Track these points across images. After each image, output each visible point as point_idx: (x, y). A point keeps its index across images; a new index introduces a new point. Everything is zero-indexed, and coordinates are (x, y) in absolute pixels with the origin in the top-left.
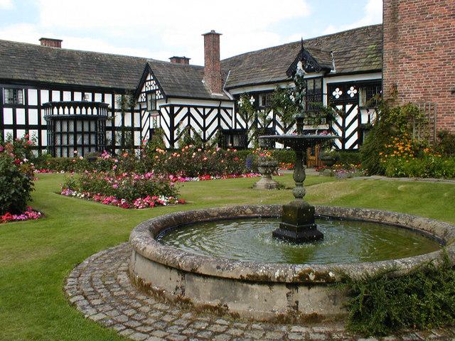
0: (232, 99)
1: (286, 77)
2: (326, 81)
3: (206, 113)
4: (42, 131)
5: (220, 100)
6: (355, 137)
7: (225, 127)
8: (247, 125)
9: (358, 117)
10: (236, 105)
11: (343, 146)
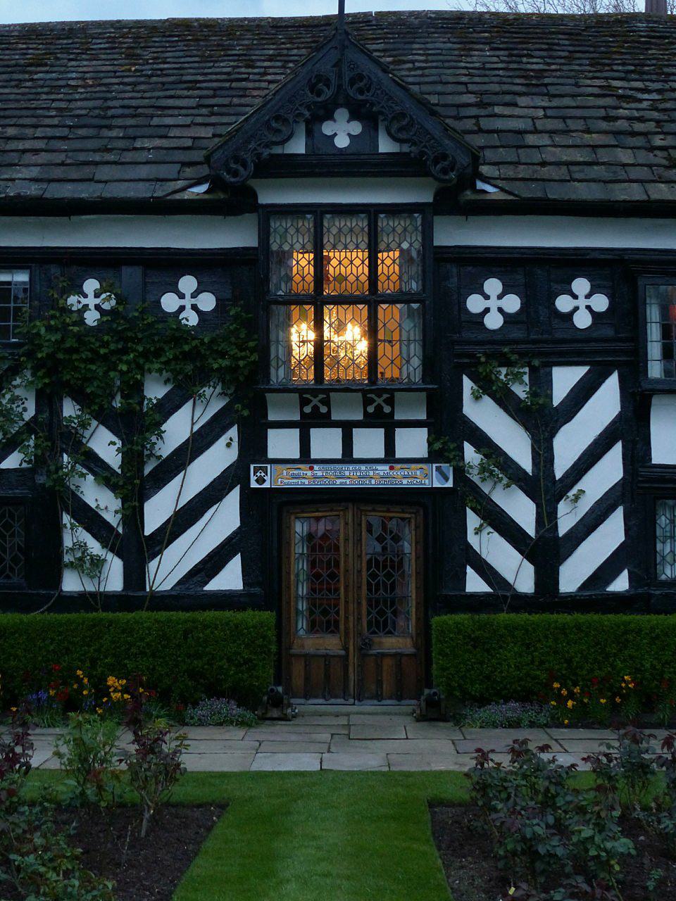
6: (611, 534)
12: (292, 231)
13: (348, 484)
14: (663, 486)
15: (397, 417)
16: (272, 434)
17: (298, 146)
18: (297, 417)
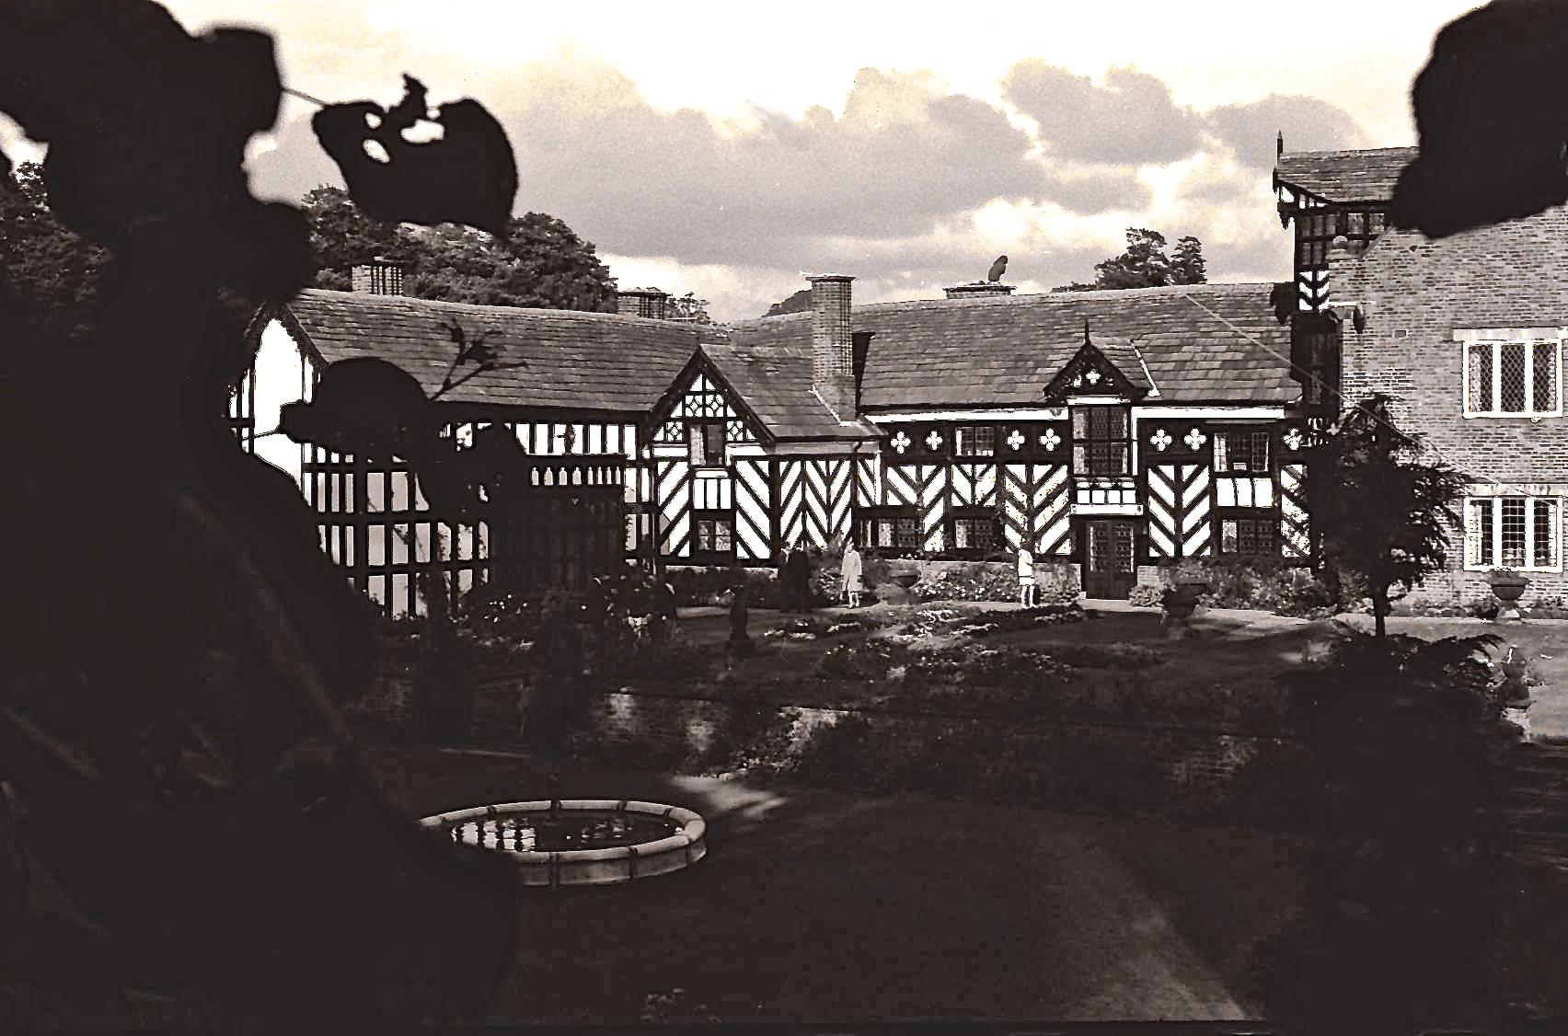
1: (1043, 399)
2: (1138, 413)
3: (925, 477)
4: (722, 415)
6: (1205, 532)
7: (864, 503)
9: (1211, 491)
16: (1080, 493)
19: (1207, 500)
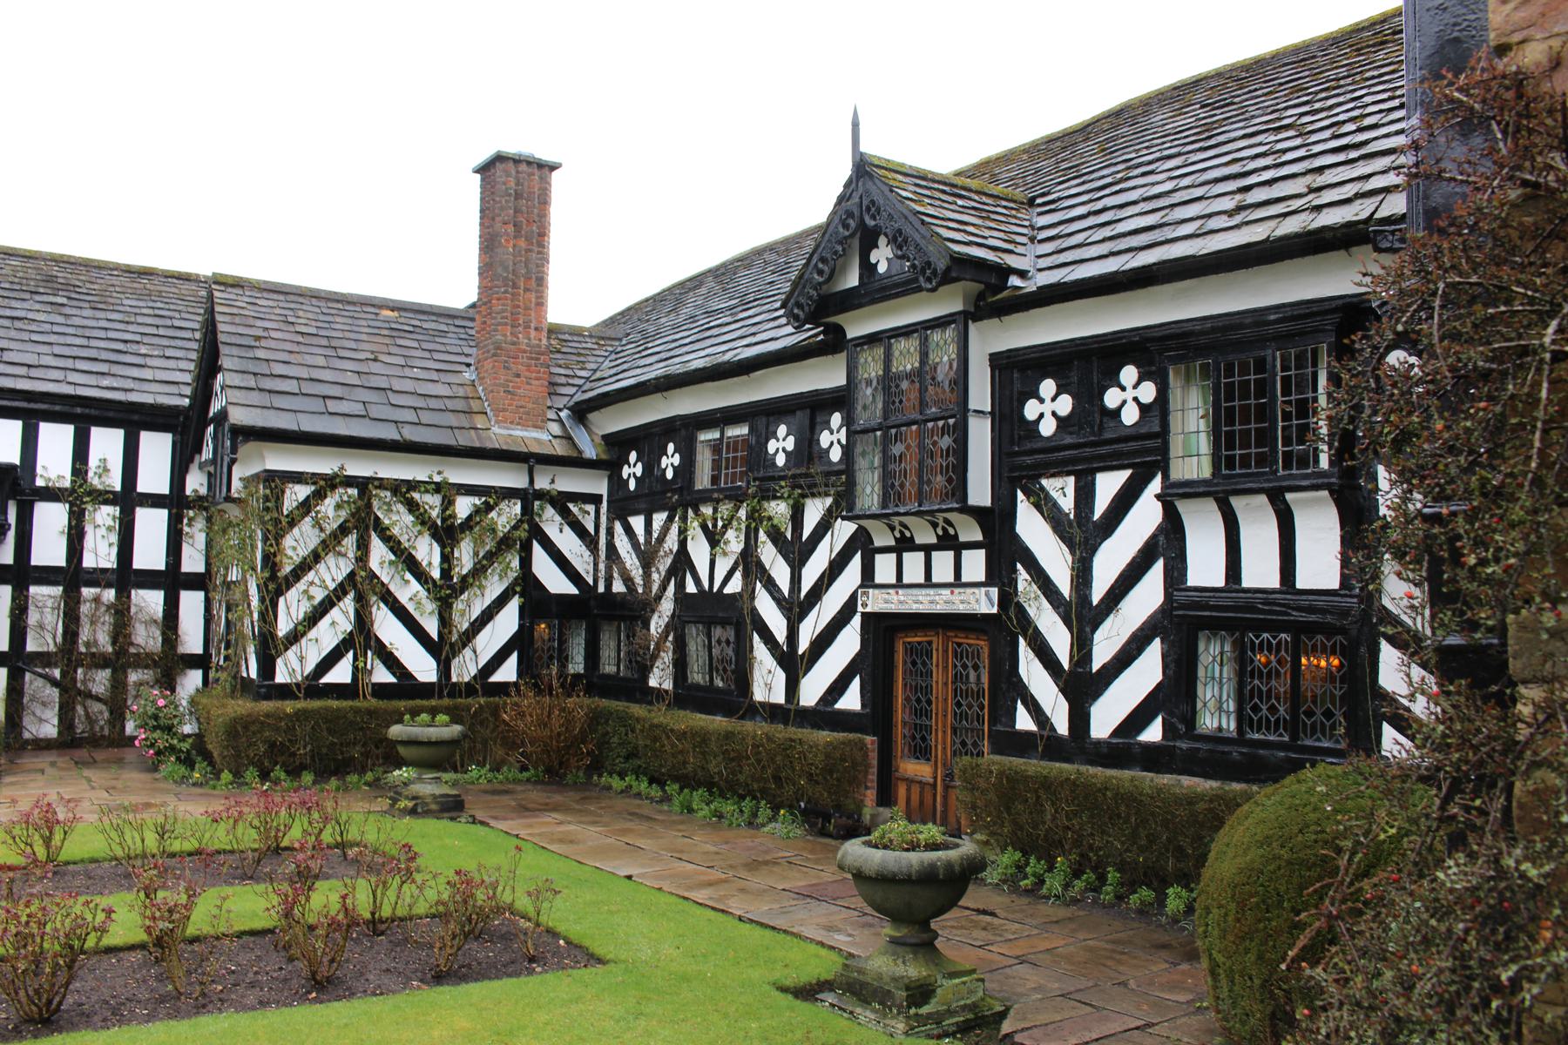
0: (590, 452)
1: (786, 336)
5: (529, 460)
6: (1147, 672)
7: (556, 582)
8: (446, 559)
10: (617, 483)
11: (1079, 718)
12: (870, 359)
13: (940, 608)
14: (1214, 614)
15: (962, 538)
17: (852, 280)
18: (892, 543)
19: (1157, 572)
